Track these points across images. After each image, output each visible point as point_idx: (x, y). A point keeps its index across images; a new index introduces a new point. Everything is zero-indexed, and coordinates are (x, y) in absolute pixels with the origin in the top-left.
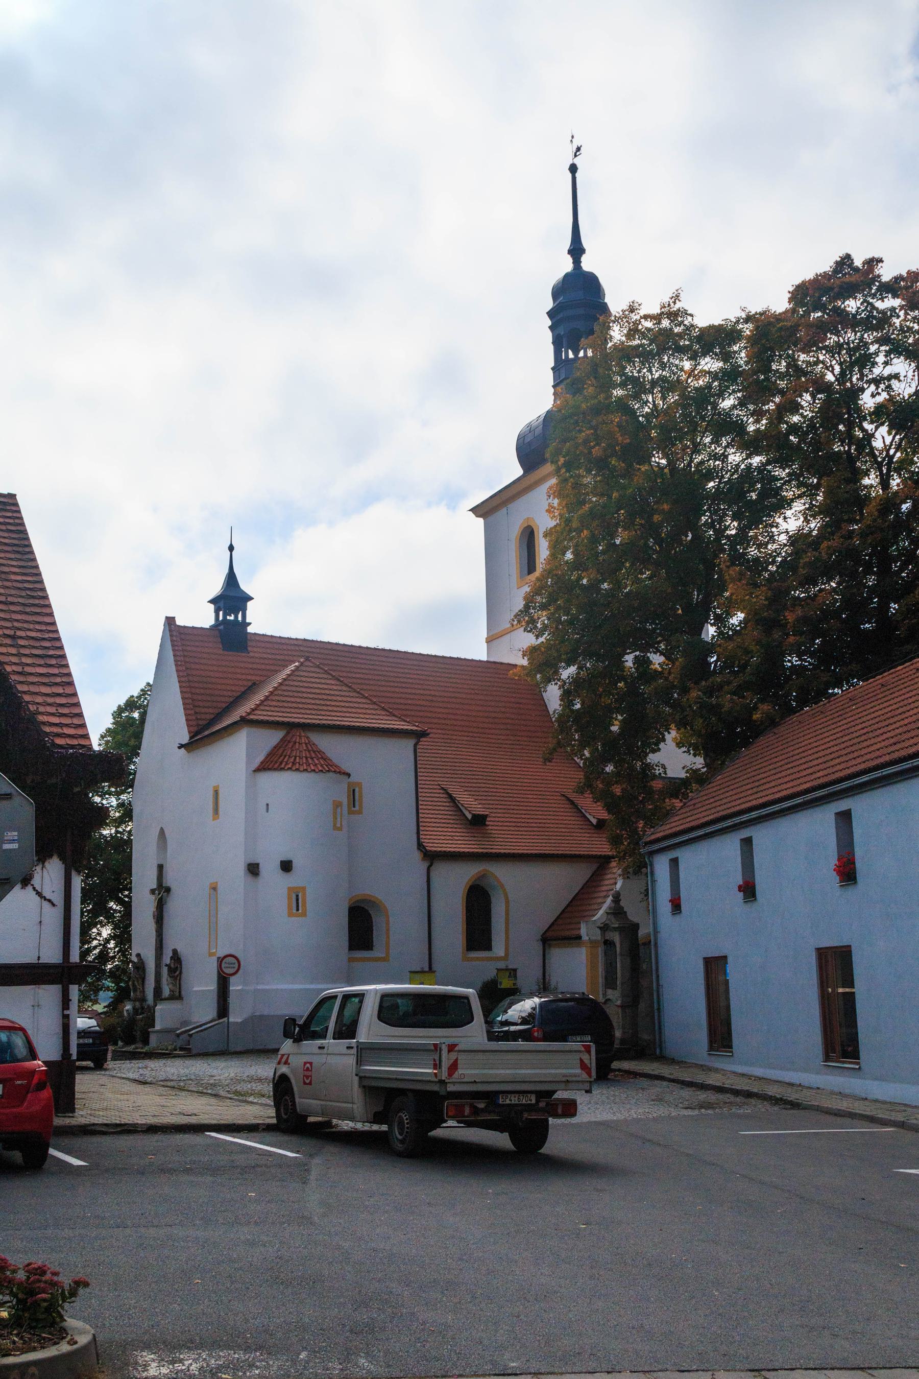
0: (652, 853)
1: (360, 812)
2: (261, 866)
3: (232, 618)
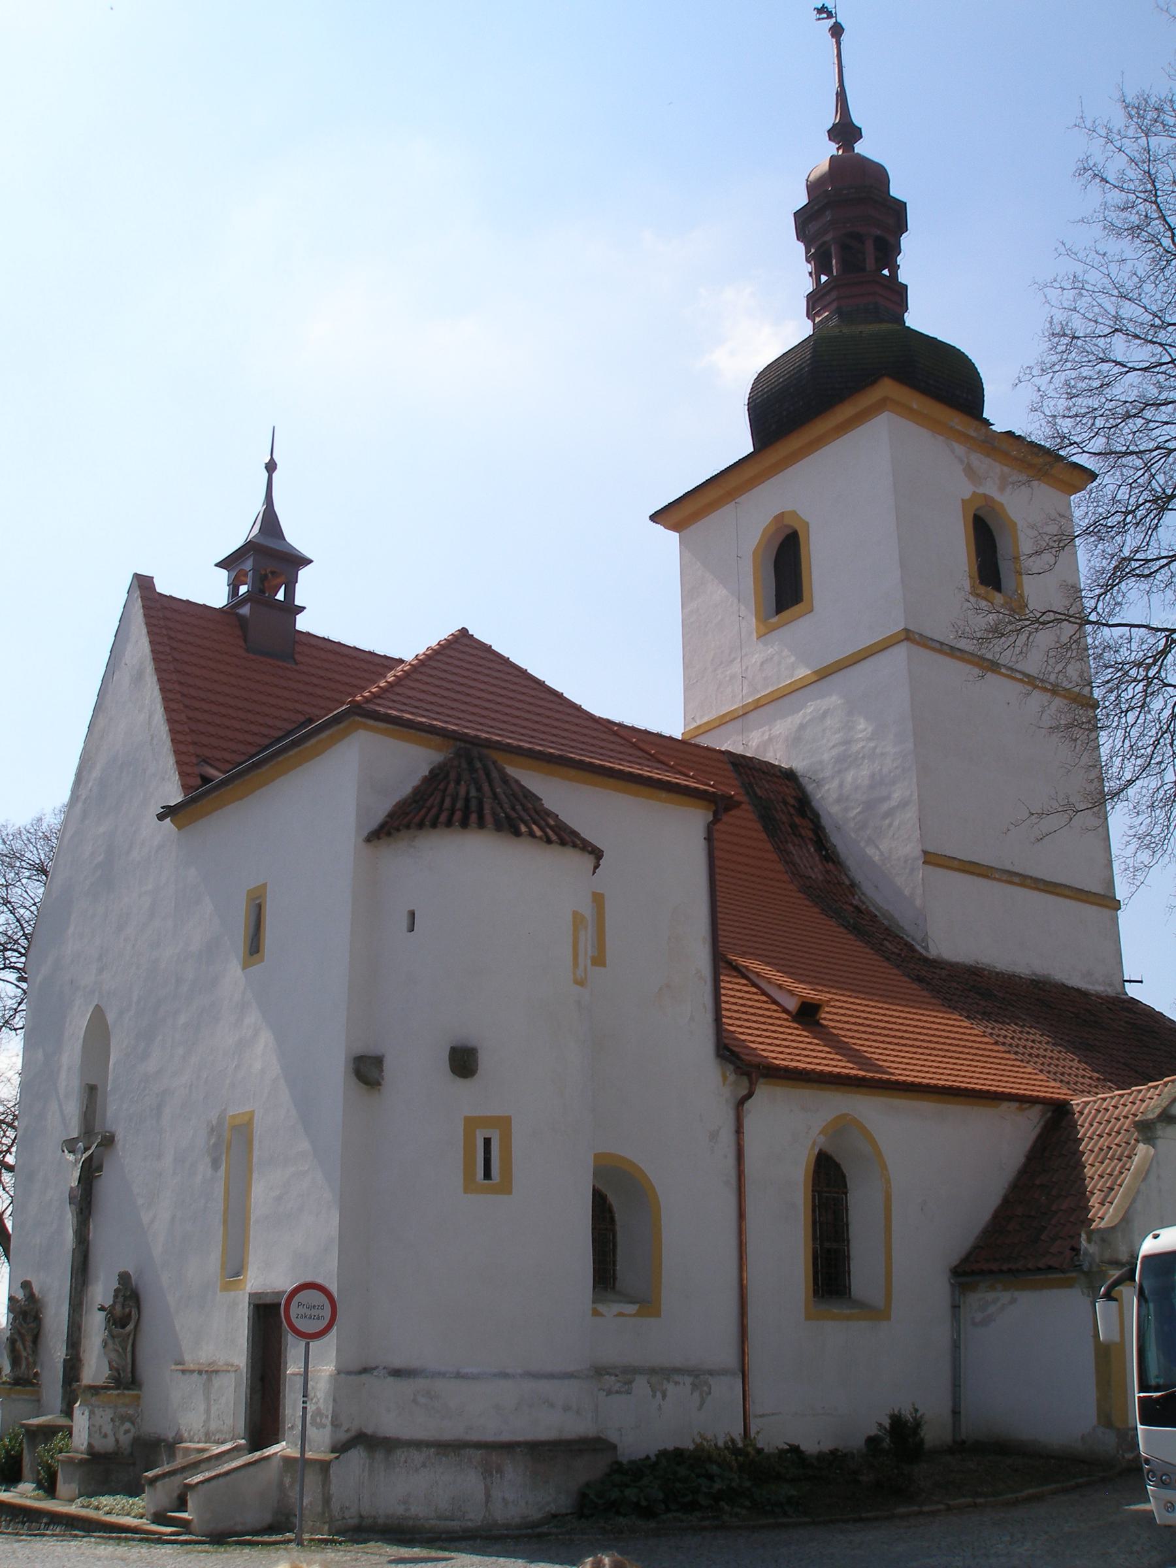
2: (388, 1064)
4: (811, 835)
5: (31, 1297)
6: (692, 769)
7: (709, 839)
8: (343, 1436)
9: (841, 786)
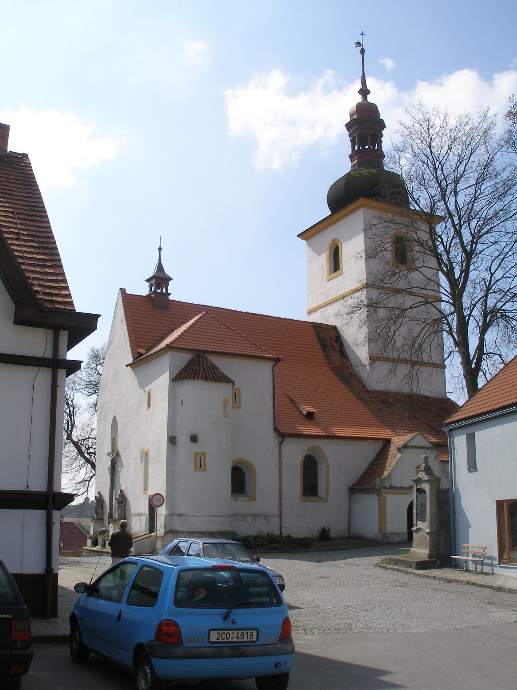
0: (450, 431)
1: (239, 407)
3: (159, 291)
4: (339, 349)
5: (100, 496)
6: (269, 350)
7: (273, 370)
8: (167, 530)
9: (348, 333)
